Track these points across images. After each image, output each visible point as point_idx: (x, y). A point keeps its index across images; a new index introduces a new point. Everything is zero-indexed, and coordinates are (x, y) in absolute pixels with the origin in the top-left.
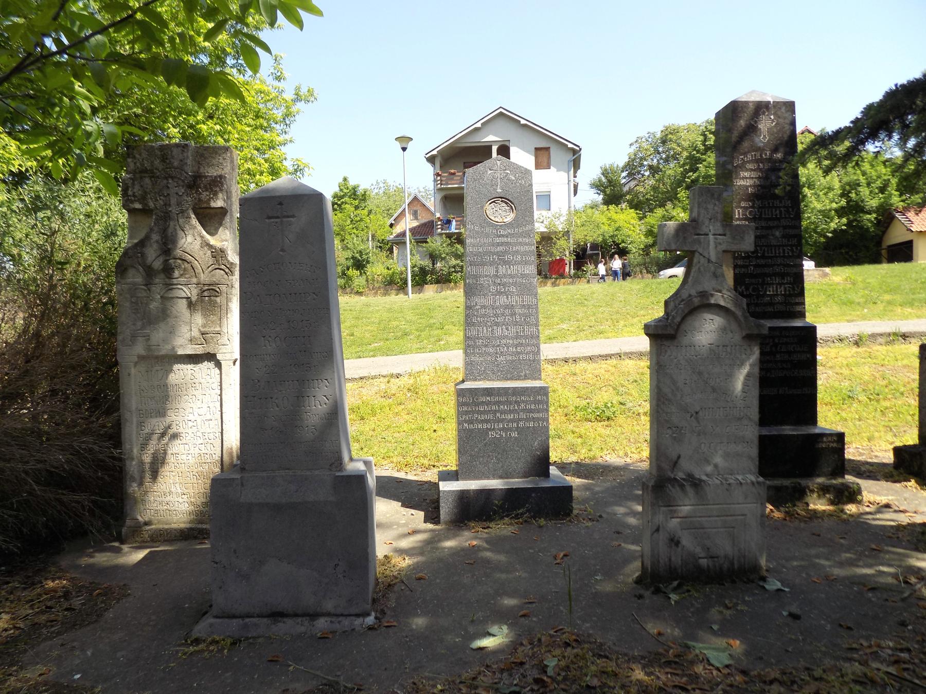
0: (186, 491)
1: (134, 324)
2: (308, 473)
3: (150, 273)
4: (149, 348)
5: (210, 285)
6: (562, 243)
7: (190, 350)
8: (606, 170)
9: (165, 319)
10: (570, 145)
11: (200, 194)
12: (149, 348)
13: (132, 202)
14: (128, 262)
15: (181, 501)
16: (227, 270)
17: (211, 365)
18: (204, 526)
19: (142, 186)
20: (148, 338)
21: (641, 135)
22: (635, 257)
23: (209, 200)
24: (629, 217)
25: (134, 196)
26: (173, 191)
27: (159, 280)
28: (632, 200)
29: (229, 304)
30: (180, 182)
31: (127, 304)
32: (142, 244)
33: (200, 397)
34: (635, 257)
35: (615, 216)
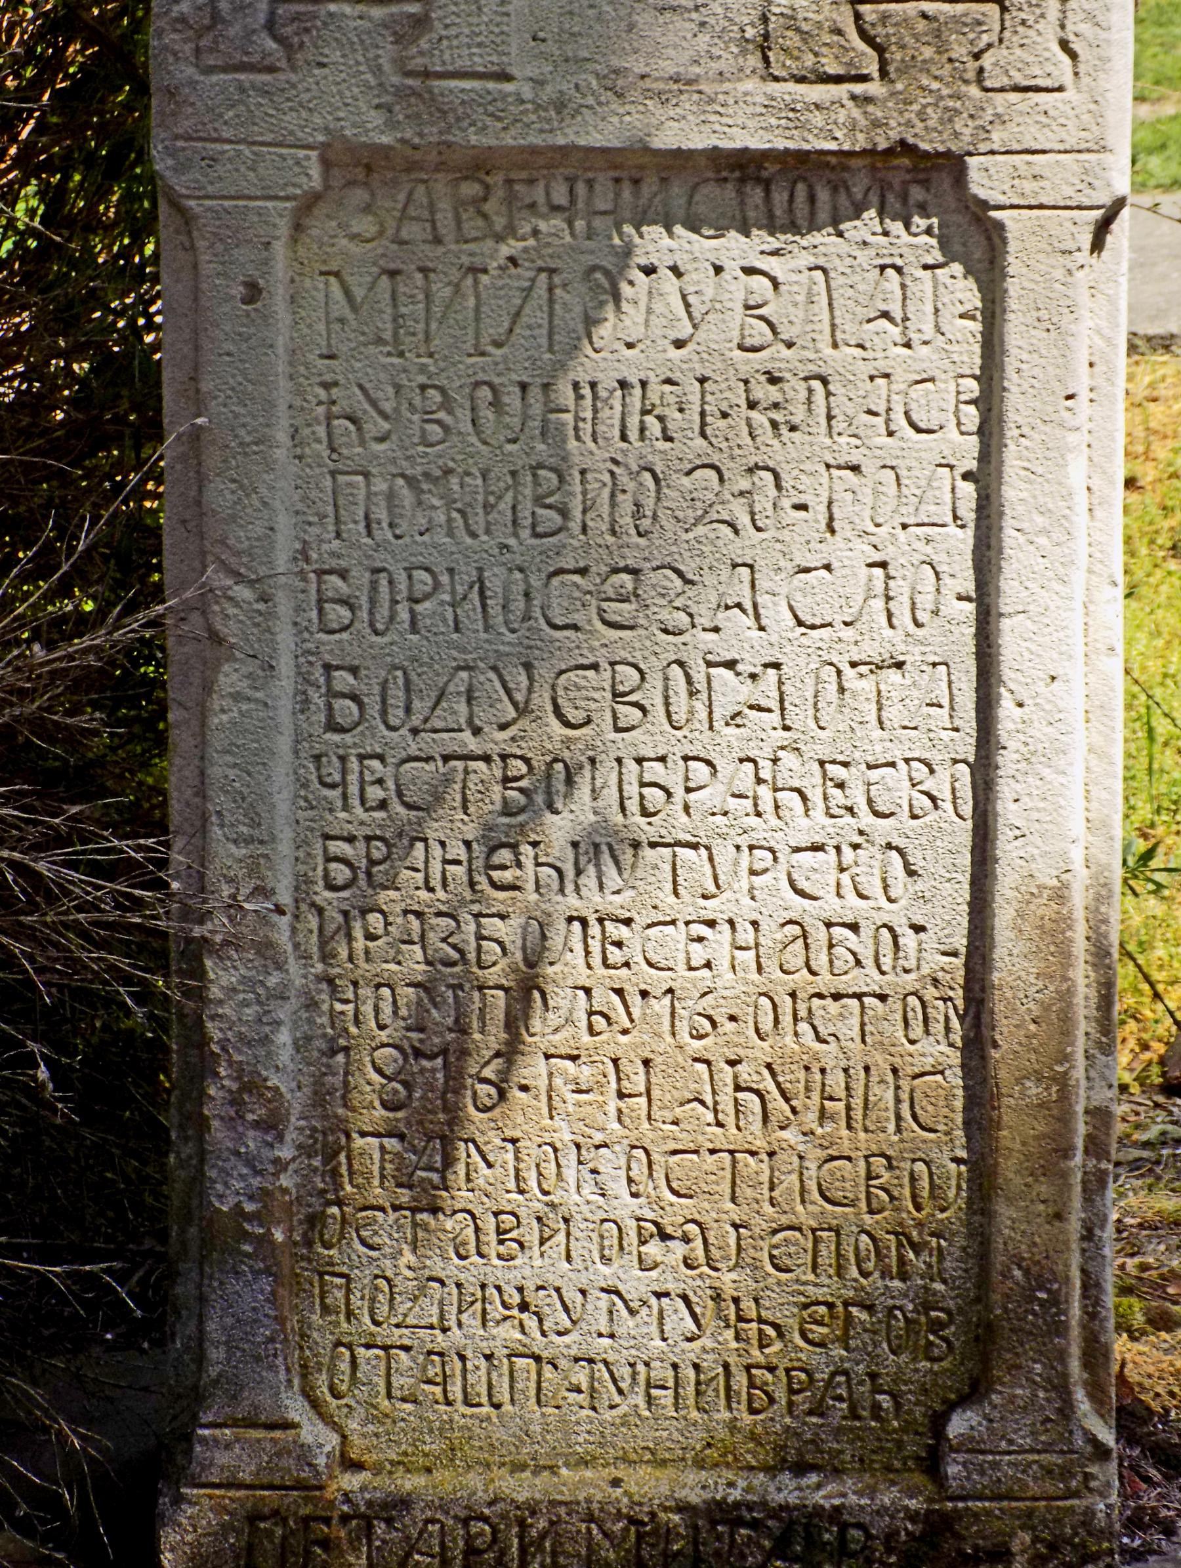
0: (675, 1212)
7: (748, 118)
12: (417, 88)
15: (636, 1284)
17: (915, 242)
18: (824, 1494)
33: (814, 487)
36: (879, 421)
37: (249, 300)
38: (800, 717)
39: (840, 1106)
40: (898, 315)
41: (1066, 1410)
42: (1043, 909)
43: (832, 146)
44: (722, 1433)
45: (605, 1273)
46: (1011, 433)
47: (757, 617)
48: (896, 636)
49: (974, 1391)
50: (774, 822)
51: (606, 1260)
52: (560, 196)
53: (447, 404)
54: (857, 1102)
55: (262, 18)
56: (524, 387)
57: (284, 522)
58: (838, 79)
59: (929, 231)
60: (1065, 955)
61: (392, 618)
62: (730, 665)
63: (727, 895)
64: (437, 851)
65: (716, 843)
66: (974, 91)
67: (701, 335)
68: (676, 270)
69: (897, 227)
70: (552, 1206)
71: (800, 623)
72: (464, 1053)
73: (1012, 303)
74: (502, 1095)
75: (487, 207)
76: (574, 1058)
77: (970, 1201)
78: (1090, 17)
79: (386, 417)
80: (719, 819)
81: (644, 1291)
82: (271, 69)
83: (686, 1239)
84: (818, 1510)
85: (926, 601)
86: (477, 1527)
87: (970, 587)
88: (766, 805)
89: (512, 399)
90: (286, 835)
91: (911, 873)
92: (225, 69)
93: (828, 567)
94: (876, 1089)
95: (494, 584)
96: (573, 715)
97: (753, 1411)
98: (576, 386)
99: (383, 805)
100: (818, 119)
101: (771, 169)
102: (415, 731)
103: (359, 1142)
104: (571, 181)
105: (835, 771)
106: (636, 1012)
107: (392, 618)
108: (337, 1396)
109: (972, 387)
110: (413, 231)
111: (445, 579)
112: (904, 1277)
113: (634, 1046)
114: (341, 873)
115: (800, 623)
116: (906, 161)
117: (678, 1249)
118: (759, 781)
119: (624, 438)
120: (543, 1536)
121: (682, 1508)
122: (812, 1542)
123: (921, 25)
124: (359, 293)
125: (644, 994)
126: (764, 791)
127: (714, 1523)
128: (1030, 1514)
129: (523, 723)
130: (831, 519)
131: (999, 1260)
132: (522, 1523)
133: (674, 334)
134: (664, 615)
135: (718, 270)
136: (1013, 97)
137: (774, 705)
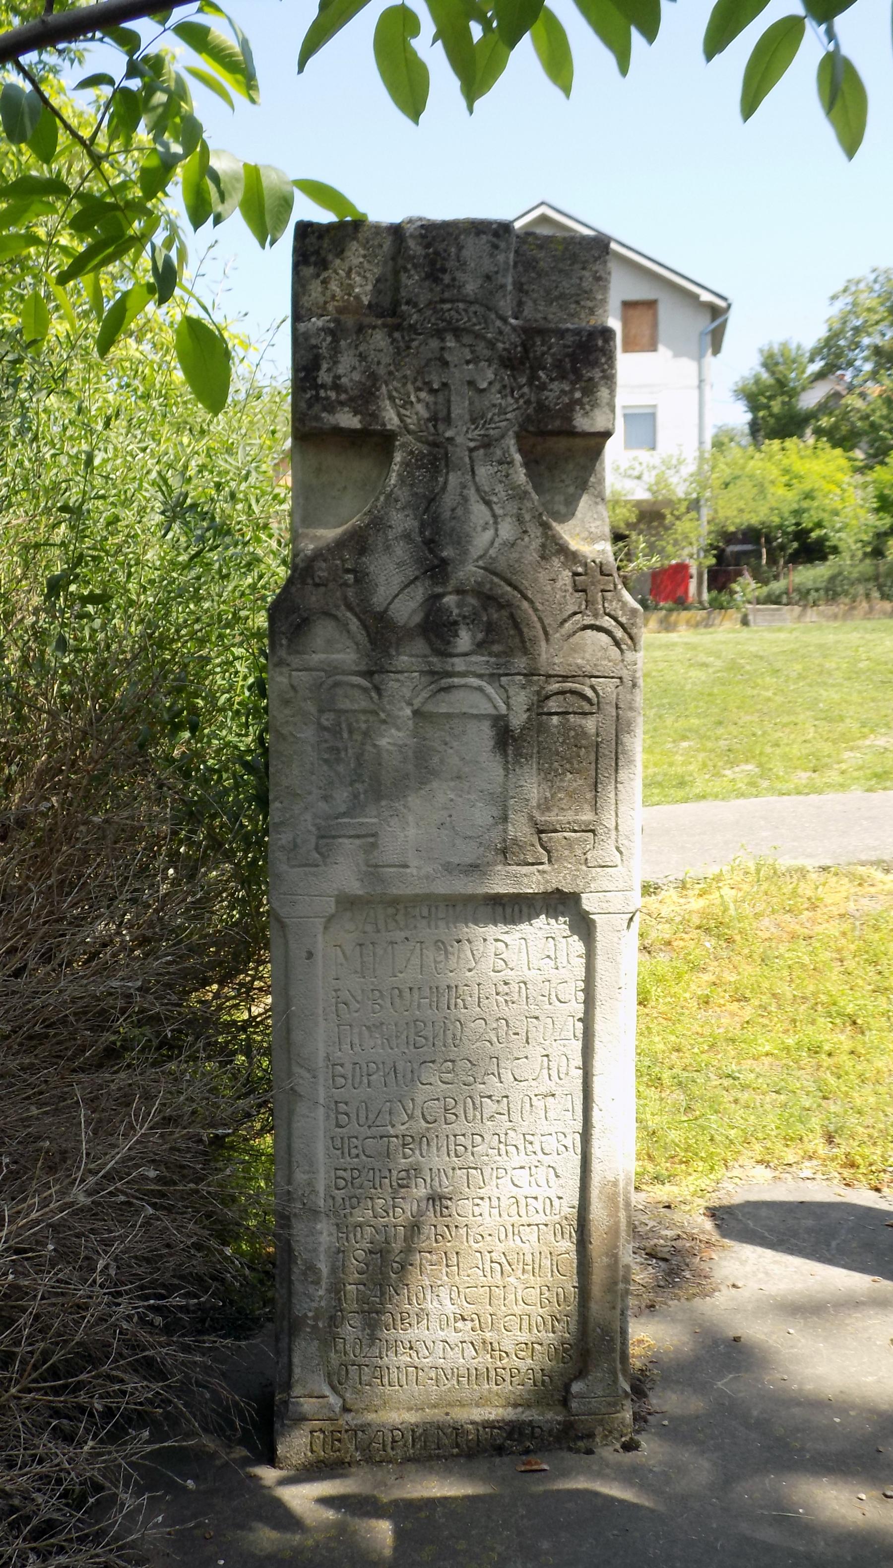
1: (326, 798)
2: (766, 1234)
3: (380, 634)
4: (373, 872)
5: (565, 678)
6: (684, 526)
8: (771, 356)
9: (423, 782)
10: (705, 297)
11: (543, 387)
12: (373, 872)
13: (330, 408)
14: (314, 599)
15: (453, 1338)
16: (619, 633)
17: (559, 926)
19: (362, 357)
20: (371, 840)
21: (856, 274)
22: (849, 560)
23: (570, 408)
24: (832, 466)
25: (337, 387)
26: (457, 375)
27: (409, 658)
28: (835, 427)
29: (626, 739)
30: (481, 347)
31: (308, 734)
32: (358, 542)
33: (521, 1026)
34: (849, 560)
35: (799, 466)
36: (546, 999)
37: (308, 959)
38: (516, 1117)
39: (530, 1268)
40: (553, 957)
41: (615, 1381)
42: (609, 1189)
43: (531, 891)
44: (486, 1393)
45: (442, 1334)
46: (598, 1003)
47: (500, 1078)
48: (552, 1084)
49: (581, 1374)
50: (506, 1158)
51: (442, 1329)
52: (425, 912)
53: (382, 996)
54: (537, 1266)
55: (313, 845)
56: (411, 989)
57: (321, 1046)
58: (533, 864)
59: (565, 923)
60: (617, 1208)
61: (361, 1083)
62: (490, 1097)
63: (488, 1187)
64: (378, 1173)
65: (484, 1168)
66: (584, 868)
67: (479, 967)
68: (468, 940)
69: (552, 921)
70: (421, 1309)
71: (516, 1080)
72: (388, 1252)
73: (599, 952)
74: (403, 1267)
75: (397, 917)
76: (430, 1252)
77: (579, 1303)
78: (627, 837)
79: (358, 1002)
80: (485, 1158)
81: (457, 1341)
82: (317, 866)
83: (472, 1320)
84: (524, 1422)
85: (563, 1070)
86: (396, 1432)
87: (580, 1064)
88: (503, 1152)
89: (407, 994)
90: (322, 1170)
91: (557, 1176)
92: (300, 866)
93: (526, 1057)
94: (544, 1261)
95: (400, 1068)
96: (429, 1118)
97: (497, 1385)
98: (431, 988)
99: (357, 1156)
100: (525, 880)
101: (506, 899)
102: (369, 1127)
103: (349, 1287)
104: (430, 907)
105: (528, 1137)
106: (453, 1234)
107: (361, 1083)
108: (341, 1384)
109: (582, 985)
110: (369, 928)
111: (381, 1066)
112: (554, 1332)
113: (453, 1247)
114: (342, 1183)
115: (516, 1080)
116: (557, 896)
117: (469, 1324)
118: (500, 1142)
119: (449, 1008)
120: (421, 1435)
121: (473, 1423)
122: (521, 1434)
123: (564, 842)
124: (348, 953)
125: (456, 1227)
126: (502, 1146)
127: (484, 1428)
128: (602, 1420)
129: (411, 1122)
130: (527, 1038)
131: (591, 1325)
132: (413, 1431)
133: (468, 967)
134: (464, 1078)
135: (485, 940)
136: (599, 869)
137: (506, 1112)
